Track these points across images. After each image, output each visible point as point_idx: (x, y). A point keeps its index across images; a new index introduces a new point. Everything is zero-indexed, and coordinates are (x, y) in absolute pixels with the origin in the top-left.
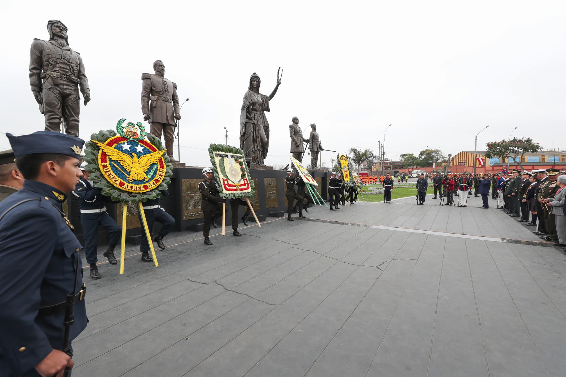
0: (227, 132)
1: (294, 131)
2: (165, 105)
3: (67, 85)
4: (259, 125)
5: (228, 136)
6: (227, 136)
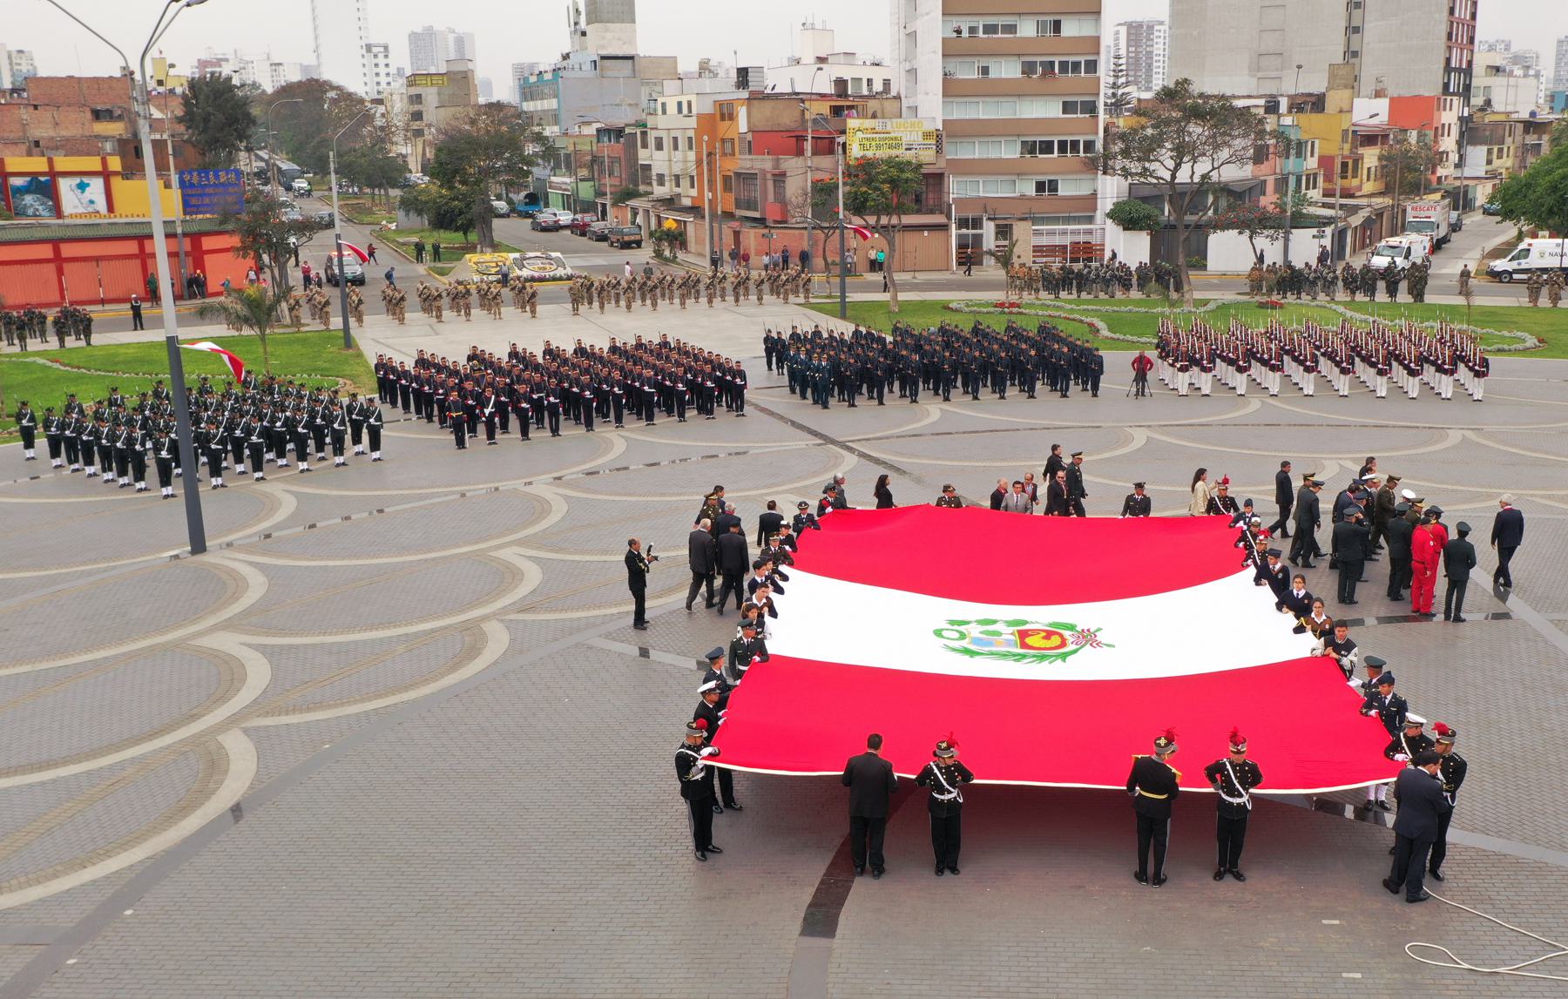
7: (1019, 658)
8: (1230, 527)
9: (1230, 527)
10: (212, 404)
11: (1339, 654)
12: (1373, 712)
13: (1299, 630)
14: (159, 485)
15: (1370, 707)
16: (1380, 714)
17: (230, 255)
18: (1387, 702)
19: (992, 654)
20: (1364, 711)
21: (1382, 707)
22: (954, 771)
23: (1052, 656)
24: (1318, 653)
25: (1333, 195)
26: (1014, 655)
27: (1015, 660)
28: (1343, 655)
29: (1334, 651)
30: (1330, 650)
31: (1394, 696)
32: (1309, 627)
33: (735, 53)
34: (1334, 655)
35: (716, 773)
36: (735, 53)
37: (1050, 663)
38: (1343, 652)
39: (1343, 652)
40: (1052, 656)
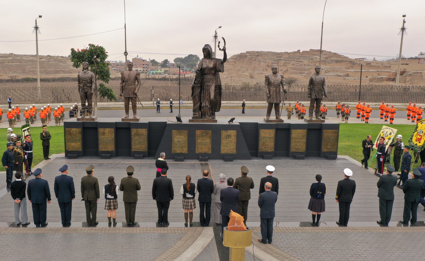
0: (404, 22)
1: (268, 82)
2: (128, 87)
3: (86, 88)
4: (208, 86)
5: (406, 30)
6: (403, 29)
17: (402, 26)
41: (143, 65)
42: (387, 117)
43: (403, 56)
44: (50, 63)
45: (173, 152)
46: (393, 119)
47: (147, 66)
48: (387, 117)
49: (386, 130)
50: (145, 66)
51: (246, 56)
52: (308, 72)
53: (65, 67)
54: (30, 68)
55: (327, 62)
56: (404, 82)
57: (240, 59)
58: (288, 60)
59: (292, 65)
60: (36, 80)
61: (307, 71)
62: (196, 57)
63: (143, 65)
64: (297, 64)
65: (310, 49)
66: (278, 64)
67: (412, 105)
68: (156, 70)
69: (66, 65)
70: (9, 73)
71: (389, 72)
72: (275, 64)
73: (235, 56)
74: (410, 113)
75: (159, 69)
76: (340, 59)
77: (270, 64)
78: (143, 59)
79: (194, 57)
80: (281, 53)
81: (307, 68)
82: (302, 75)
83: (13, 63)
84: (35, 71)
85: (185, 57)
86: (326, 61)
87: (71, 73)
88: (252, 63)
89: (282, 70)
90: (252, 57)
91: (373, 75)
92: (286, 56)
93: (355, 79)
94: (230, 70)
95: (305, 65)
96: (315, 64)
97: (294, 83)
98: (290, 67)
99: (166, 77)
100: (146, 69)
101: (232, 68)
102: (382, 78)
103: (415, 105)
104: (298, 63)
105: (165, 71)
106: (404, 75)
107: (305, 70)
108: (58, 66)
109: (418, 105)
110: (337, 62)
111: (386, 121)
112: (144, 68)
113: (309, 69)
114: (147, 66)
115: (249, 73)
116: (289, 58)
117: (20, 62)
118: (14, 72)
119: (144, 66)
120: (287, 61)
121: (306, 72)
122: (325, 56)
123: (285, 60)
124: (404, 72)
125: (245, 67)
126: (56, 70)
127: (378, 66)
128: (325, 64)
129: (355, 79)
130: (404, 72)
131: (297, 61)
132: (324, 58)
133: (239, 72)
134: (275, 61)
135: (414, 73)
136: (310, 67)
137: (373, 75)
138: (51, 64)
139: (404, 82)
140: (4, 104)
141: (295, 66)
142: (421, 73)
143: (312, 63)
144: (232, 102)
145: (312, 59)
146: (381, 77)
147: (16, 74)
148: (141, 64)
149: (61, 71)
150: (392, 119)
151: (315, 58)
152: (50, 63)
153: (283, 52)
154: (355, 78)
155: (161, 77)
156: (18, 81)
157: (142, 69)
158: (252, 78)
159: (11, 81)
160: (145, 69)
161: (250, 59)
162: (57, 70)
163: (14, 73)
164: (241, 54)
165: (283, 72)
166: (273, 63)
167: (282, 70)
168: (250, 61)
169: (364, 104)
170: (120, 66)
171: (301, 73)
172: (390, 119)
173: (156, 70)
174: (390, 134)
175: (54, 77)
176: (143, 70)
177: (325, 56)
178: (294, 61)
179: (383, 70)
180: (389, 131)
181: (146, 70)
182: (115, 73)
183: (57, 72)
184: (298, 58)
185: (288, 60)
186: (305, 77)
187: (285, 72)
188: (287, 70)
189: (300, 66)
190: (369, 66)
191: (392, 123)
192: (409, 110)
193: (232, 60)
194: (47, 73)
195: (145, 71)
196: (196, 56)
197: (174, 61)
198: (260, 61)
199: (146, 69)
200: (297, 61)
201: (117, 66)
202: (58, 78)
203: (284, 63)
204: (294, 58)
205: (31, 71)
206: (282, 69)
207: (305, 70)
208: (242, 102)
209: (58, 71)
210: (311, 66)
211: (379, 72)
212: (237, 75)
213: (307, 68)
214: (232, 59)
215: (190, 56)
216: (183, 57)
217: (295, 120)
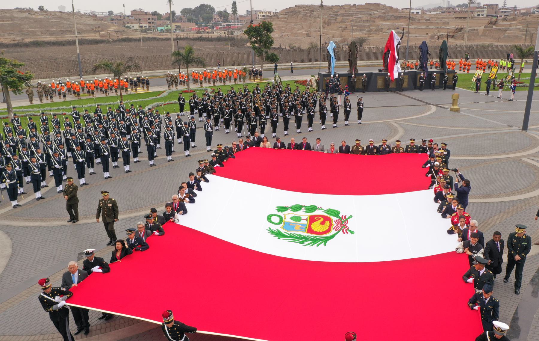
7: (302, 240)
8: (423, 167)
9: (423, 167)
10: (227, 113)
11: (471, 251)
12: (476, 308)
13: (451, 232)
14: (308, 126)
15: (475, 303)
16: (481, 309)
18: (486, 301)
19: (291, 237)
20: (471, 305)
21: (482, 303)
22: (176, 331)
23: (320, 240)
24: (460, 251)
25: (482, 14)
26: (302, 238)
27: (301, 243)
28: (474, 253)
29: (470, 251)
30: (467, 249)
31: (491, 298)
32: (456, 231)
33: (124, 6)
34: (469, 253)
35: (71, 315)
36: (124, 6)
37: (317, 246)
38: (474, 251)
39: (474, 251)
40: (320, 240)
41: (149, 19)
42: (464, 69)
43: (451, 4)
44: (50, 21)
45: (378, 88)
46: (469, 70)
47: (153, 21)
48: (464, 69)
49: (478, 72)
50: (151, 21)
51: (299, 12)
52: (368, 29)
53: (70, 26)
54: (28, 28)
55: (386, 19)
56: (462, 38)
57: (293, 15)
58: (346, 16)
59: (351, 21)
60: (74, 43)
61: (366, 28)
62: (210, 7)
63: (149, 19)
64: (356, 20)
65: (366, 3)
66: (336, 21)
67: (480, 60)
68: (165, 26)
69: (71, 23)
70: (4, 35)
71: (448, 29)
72: (332, 20)
73: (284, 10)
74: (478, 66)
75: (168, 24)
76: (396, 14)
77: (327, 20)
78: (146, 11)
79: (208, 8)
80: (332, 6)
81: (366, 24)
82: (362, 33)
83: (3, 21)
84: (36, 32)
85: (196, 8)
86: (385, 17)
87: (79, 33)
88: (307, 19)
89: (341, 27)
90: (306, 13)
91: (433, 32)
92: (342, 11)
93: (416, 36)
94: (283, 27)
95: (364, 22)
96: (373, 20)
97: (365, 42)
98: (349, 24)
99: (203, 36)
100: (153, 25)
101: (285, 25)
102: (442, 35)
103: (493, 60)
104: (356, 19)
105: (176, 28)
106: (462, 32)
107: (364, 27)
108: (62, 25)
109: (483, 60)
110: (396, 17)
111: (464, 72)
112: (150, 23)
113: (368, 26)
114: (153, 21)
115: (306, 31)
116: (346, 14)
117: (12, 21)
118: (10, 33)
119: (149, 21)
120: (345, 17)
121: (366, 29)
122: (383, 11)
123: (342, 16)
124: (462, 29)
125: (299, 24)
126: (61, 30)
127: (437, 23)
128: (385, 20)
129: (416, 36)
130: (462, 29)
131: (355, 17)
132: (382, 14)
133: (293, 30)
134: (332, 17)
135: (471, 30)
136: (370, 24)
137: (433, 32)
138: (52, 22)
139: (462, 38)
140: (152, 70)
141: (354, 23)
142: (477, 30)
143: (370, 19)
144: (377, 61)
145: (370, 15)
146: (441, 33)
147: (14, 36)
148: (146, 19)
149: (66, 30)
150: (468, 70)
151: (373, 13)
152: (50, 21)
153: (334, 5)
154: (416, 35)
155: (197, 37)
156: (27, 45)
157: (147, 25)
158: (309, 37)
159: (18, 45)
160: (152, 25)
161: (305, 15)
162: (62, 30)
163: (10, 36)
164: (290, 8)
165: (342, 29)
166: (330, 19)
167: (341, 27)
168: (304, 17)
169: (481, 60)
170: (117, 20)
171: (360, 31)
172: (468, 70)
173: (165, 26)
174: (480, 73)
175: (68, 39)
176: (149, 27)
177: (383, 11)
178: (352, 16)
179: (442, 27)
180: (480, 72)
181: (153, 27)
182: (133, 32)
183: (63, 32)
184: (356, 14)
185: (346, 16)
186: (365, 35)
187: (344, 29)
188: (346, 27)
189: (359, 22)
190: (429, 22)
191: (468, 73)
192: (478, 64)
193: (282, 16)
194: (51, 34)
195: (152, 27)
196: (210, 5)
197: (181, 12)
198: (315, 17)
199: (153, 25)
200: (355, 17)
201: (112, 21)
202: (73, 41)
203: (342, 20)
204: (352, 14)
205: (31, 32)
206: (341, 26)
207: (364, 27)
208: (290, 64)
209: (63, 31)
210: (370, 22)
211: (439, 29)
212: (292, 33)
213: (366, 24)
214: (282, 14)
215: (203, 6)
216: (193, 8)
217: (434, 70)
